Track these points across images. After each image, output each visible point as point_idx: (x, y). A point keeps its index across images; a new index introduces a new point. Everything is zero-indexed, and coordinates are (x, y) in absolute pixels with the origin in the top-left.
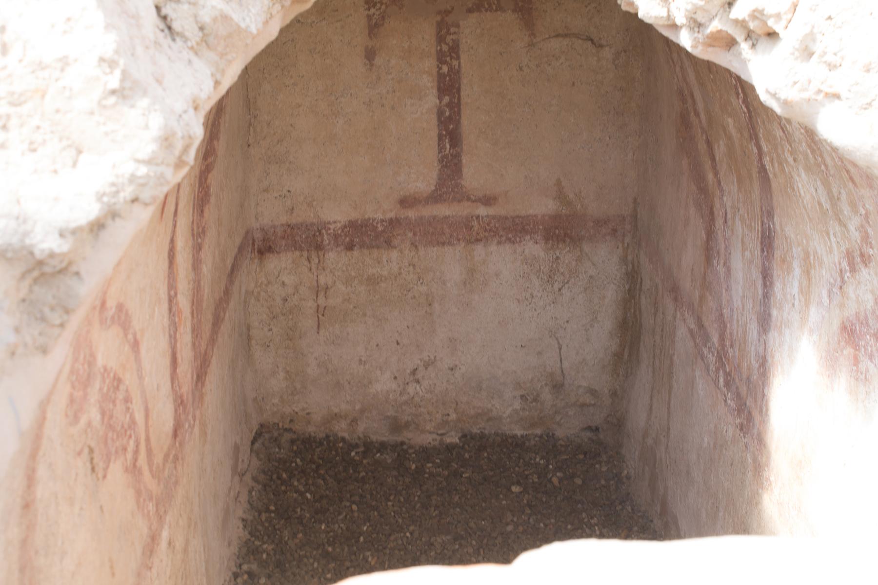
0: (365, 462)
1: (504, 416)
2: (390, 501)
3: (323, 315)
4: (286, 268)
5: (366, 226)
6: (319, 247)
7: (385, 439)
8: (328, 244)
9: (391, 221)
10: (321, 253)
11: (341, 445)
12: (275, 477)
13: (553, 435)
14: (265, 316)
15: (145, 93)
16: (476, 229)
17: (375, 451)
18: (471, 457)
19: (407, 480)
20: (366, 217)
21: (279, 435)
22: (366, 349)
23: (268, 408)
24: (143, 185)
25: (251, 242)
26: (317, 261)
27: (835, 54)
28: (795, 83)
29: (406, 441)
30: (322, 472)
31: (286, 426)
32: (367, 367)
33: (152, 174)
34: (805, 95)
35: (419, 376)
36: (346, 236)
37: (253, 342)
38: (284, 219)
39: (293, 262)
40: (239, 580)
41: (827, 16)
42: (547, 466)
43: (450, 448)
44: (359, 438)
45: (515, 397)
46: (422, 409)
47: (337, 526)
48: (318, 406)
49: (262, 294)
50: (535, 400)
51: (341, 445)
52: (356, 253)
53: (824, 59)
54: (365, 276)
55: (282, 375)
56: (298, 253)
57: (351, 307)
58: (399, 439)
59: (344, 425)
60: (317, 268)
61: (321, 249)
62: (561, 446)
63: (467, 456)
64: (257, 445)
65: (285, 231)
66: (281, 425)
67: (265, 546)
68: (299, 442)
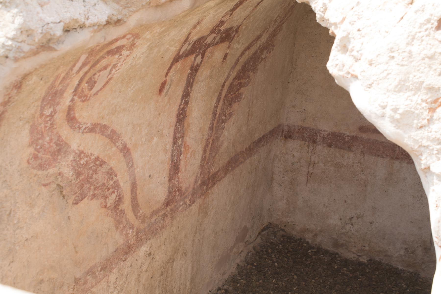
0: (314, 257)
1: (395, 256)
2: (314, 279)
3: (310, 177)
4: (296, 148)
5: (340, 137)
6: (314, 142)
7: (329, 249)
8: (319, 141)
9: (353, 137)
10: (315, 145)
11: (305, 245)
12: (264, 250)
13: (419, 274)
14: (282, 169)
15: (17, 7)
16: (397, 152)
17: (321, 253)
18: (369, 272)
19: (329, 272)
20: (341, 132)
21: (278, 231)
22: (329, 200)
23: (275, 216)
24: (10, 50)
25: (281, 131)
26: (312, 148)
27: (358, 52)
28: (337, 65)
29: (339, 253)
30: (289, 255)
31: (282, 228)
32: (328, 209)
33: (14, 46)
34: (341, 73)
35: (353, 221)
36: (329, 139)
37: (274, 181)
38: (300, 123)
39: (300, 146)
40: (219, 292)
41: (357, 29)
42: (407, 289)
43: (360, 264)
44: (316, 245)
45: (402, 248)
46: (352, 240)
47: (281, 282)
48: (298, 222)
49: (283, 158)
50: (413, 253)
51: (305, 245)
52: (332, 149)
53: (352, 54)
54: (335, 163)
55: (285, 201)
56: (303, 142)
57: (325, 176)
58: (336, 251)
59: (310, 235)
60: (312, 152)
61: (315, 143)
62: (420, 281)
63: (367, 271)
64: (264, 232)
65: (299, 129)
66: (280, 226)
67: (242, 281)
68: (285, 237)
